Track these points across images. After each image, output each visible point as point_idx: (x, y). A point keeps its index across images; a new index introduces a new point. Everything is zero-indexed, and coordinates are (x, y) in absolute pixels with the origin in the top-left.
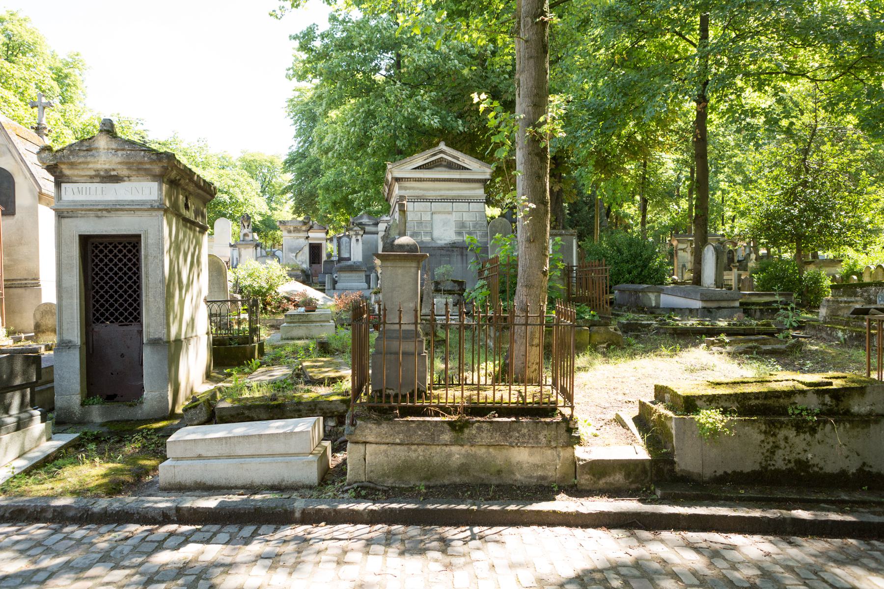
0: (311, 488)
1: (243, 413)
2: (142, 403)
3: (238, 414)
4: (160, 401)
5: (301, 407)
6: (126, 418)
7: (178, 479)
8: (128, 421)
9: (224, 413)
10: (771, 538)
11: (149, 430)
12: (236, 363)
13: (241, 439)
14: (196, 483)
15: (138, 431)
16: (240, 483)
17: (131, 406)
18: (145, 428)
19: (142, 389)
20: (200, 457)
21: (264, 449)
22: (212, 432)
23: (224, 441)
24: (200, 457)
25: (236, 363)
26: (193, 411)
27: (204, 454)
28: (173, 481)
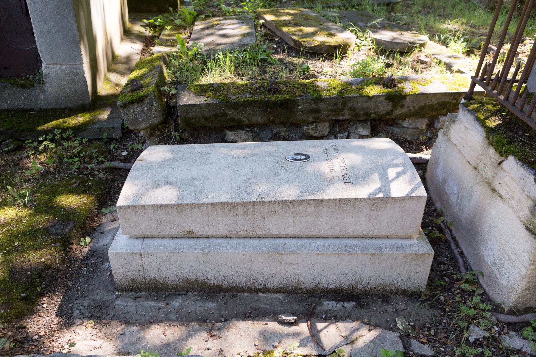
0: (412, 295)
1: (225, 115)
2: (41, 82)
3: (216, 116)
4: (73, 81)
5: (322, 106)
6: (21, 106)
7: (152, 273)
8: (24, 111)
9: (192, 114)
10: (142, 34)
11: (64, 130)
12: (155, 9)
13: (277, 207)
14: (187, 281)
15: (46, 132)
16: (274, 283)
17: (24, 86)
18: (58, 127)
19: (35, 60)
20: (190, 235)
21: (325, 224)
22: (85, 49)
23: (241, 209)
24: (190, 235)
25: (155, 9)
26: (136, 108)
27: (198, 230)
28: (141, 278)
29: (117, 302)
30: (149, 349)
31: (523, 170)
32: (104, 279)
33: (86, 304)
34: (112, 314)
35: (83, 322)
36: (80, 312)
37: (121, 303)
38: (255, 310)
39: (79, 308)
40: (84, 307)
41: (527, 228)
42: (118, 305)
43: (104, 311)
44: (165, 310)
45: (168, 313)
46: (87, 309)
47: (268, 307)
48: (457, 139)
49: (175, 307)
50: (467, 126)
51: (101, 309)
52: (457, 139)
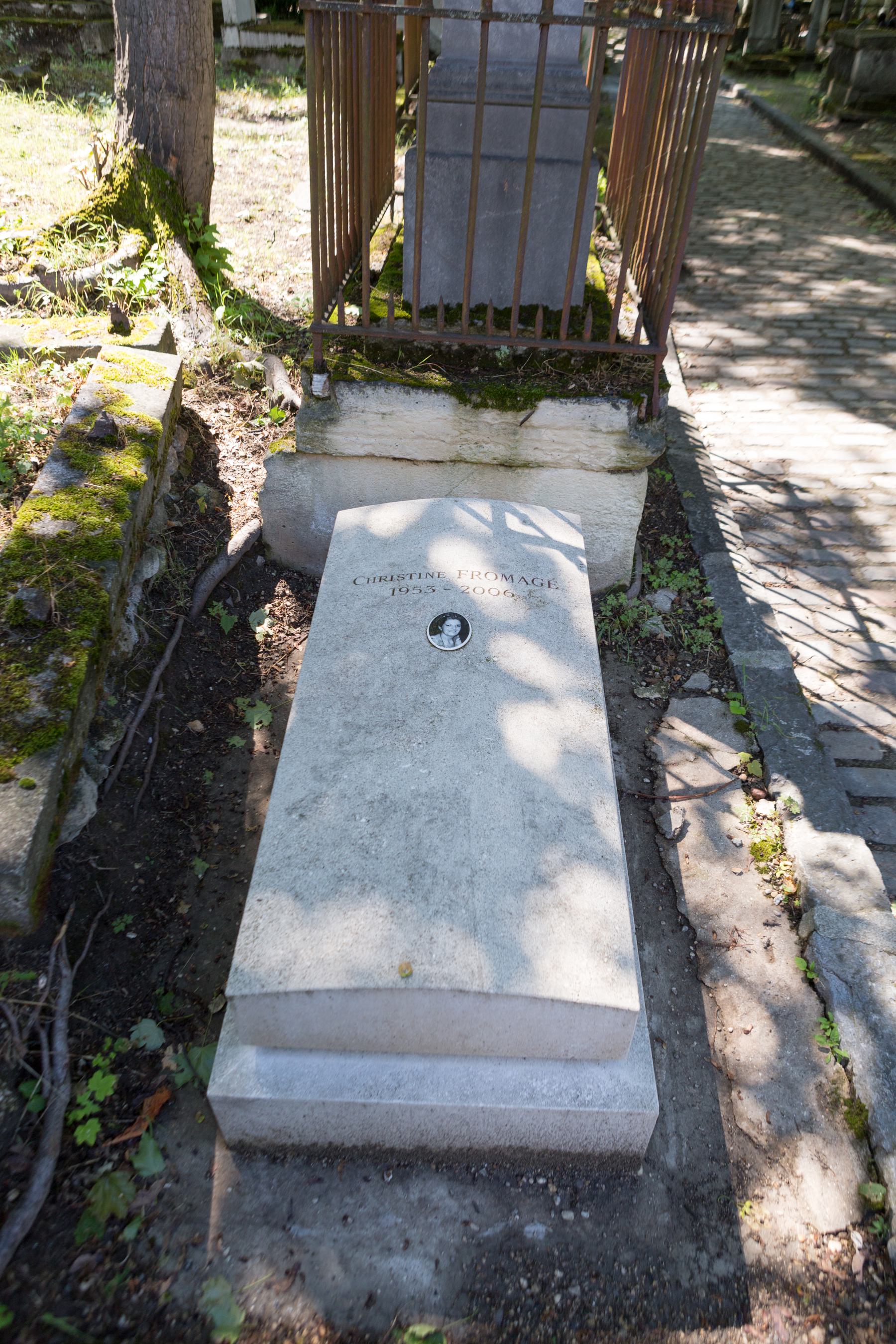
29: (671, 1162)
30: (797, 1050)
31: (582, 406)
32: (589, 1226)
33: (690, 1250)
34: (707, 1167)
35: (751, 1235)
36: (719, 1255)
37: (673, 1151)
38: (647, 878)
39: (704, 1264)
40: (699, 1249)
41: (614, 471)
42: (679, 1158)
43: (704, 1190)
44: (677, 1043)
45: (685, 1036)
46: (704, 1240)
47: (637, 857)
48: (364, 445)
49: (666, 1022)
50: (384, 409)
51: (696, 1200)
52: (364, 445)
